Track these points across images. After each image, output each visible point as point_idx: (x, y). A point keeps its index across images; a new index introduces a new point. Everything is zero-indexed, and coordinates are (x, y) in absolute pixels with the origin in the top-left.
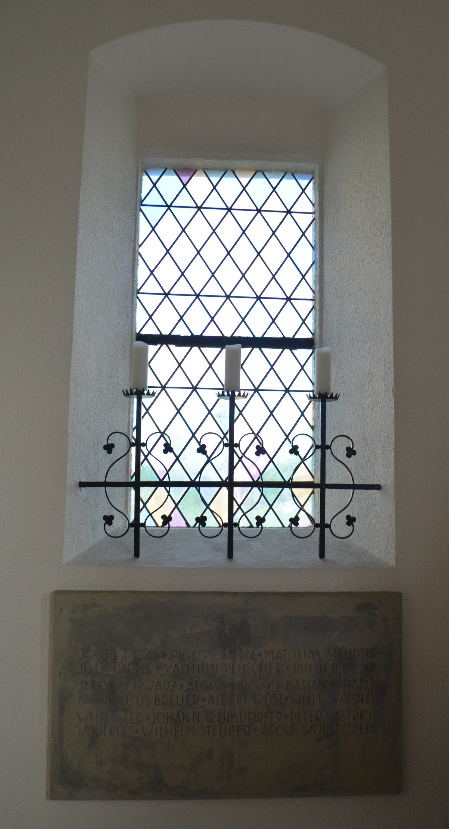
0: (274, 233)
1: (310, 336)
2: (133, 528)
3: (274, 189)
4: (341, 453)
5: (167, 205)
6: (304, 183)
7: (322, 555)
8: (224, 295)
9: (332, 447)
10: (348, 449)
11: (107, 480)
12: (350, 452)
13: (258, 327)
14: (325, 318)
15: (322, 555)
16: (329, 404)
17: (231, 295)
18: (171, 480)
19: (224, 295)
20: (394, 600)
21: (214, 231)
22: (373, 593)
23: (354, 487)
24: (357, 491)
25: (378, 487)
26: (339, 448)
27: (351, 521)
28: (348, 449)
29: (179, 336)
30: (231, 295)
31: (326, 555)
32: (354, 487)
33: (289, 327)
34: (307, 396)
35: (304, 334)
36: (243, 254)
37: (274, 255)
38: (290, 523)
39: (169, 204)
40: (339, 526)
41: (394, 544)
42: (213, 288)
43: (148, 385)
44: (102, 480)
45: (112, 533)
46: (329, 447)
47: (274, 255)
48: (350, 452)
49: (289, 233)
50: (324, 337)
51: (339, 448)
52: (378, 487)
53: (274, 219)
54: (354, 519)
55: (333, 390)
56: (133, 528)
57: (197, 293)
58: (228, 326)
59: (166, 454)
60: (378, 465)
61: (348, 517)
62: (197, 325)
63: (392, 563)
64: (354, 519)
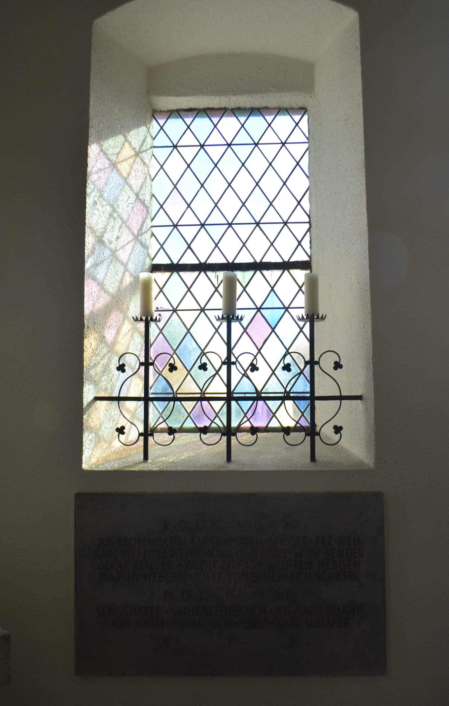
0: (270, 164)
1: (306, 258)
2: (143, 437)
3: (243, 126)
5: (255, 143)
6: (297, 118)
8: (200, 223)
11: (339, 401)
12: (338, 366)
13: (258, 251)
17: (178, 224)
18: (342, 395)
19: (254, 222)
21: (189, 166)
24: (115, 394)
27: (338, 429)
29: (270, 262)
30: (178, 224)
33: (286, 250)
34: (215, 317)
35: (301, 256)
36: (216, 185)
37: (271, 184)
38: (291, 433)
39: (256, 142)
42: (216, 217)
43: (237, 307)
44: (343, 401)
46: (318, 363)
47: (271, 184)
48: (338, 366)
49: (284, 164)
51: (327, 362)
53: (189, 153)
54: (341, 428)
56: (143, 437)
57: (258, 221)
58: (230, 251)
59: (168, 371)
60: (355, 378)
62: (203, 251)
64: (341, 428)
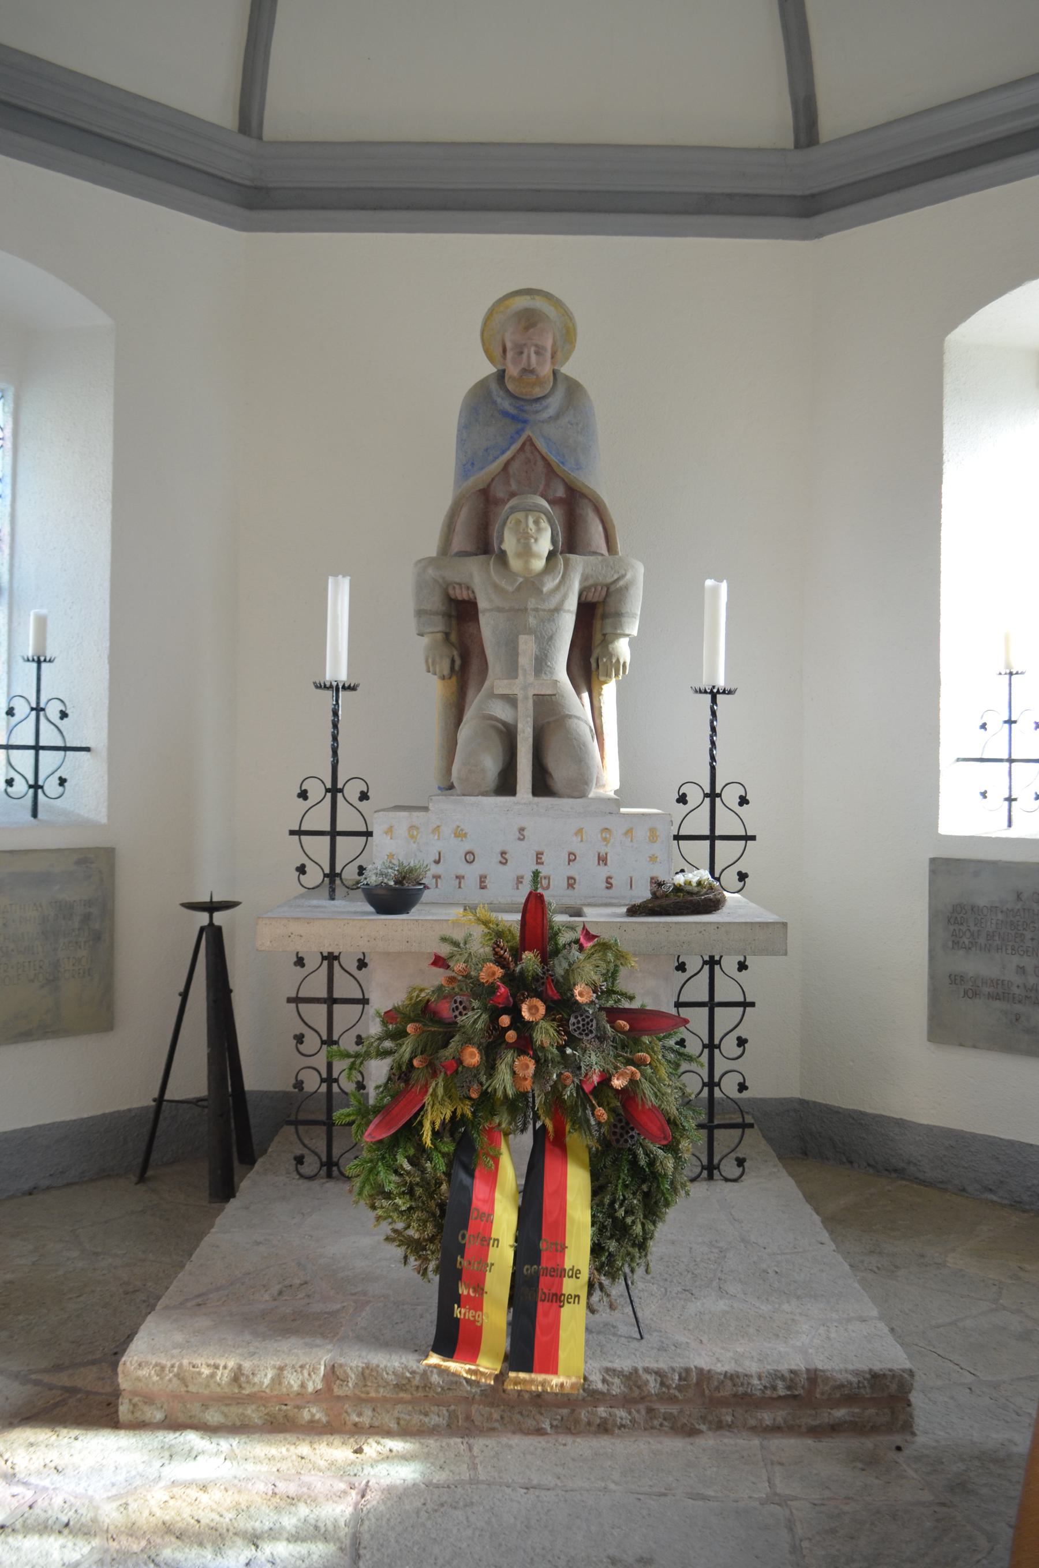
4: (54, 716)
7: (35, 814)
9: (345, 791)
10: (61, 712)
14: (16, 565)
15: (35, 814)
16: (44, 665)
20: (109, 854)
22: (88, 849)
23: (65, 749)
25: (87, 749)
26: (352, 791)
27: (62, 781)
28: (61, 712)
31: (40, 815)
32: (65, 749)
40: (51, 787)
41: (106, 804)
45: (476, 1209)
48: (364, 796)
50: (15, 586)
52: (87, 749)
54: (746, 1041)
55: (1007, 803)
60: (90, 726)
61: (60, 778)
63: (104, 820)
64: (746, 1041)
